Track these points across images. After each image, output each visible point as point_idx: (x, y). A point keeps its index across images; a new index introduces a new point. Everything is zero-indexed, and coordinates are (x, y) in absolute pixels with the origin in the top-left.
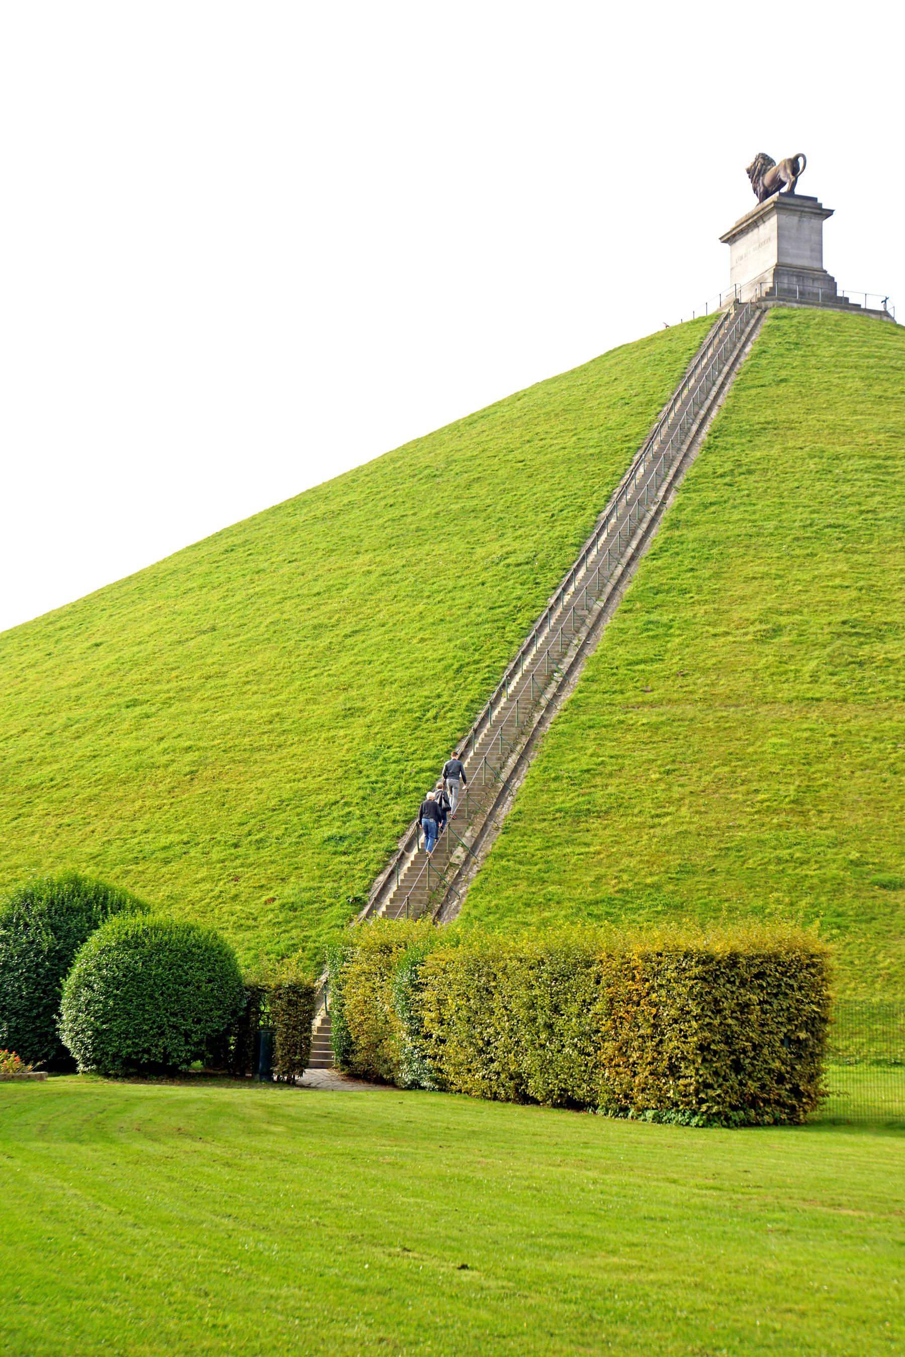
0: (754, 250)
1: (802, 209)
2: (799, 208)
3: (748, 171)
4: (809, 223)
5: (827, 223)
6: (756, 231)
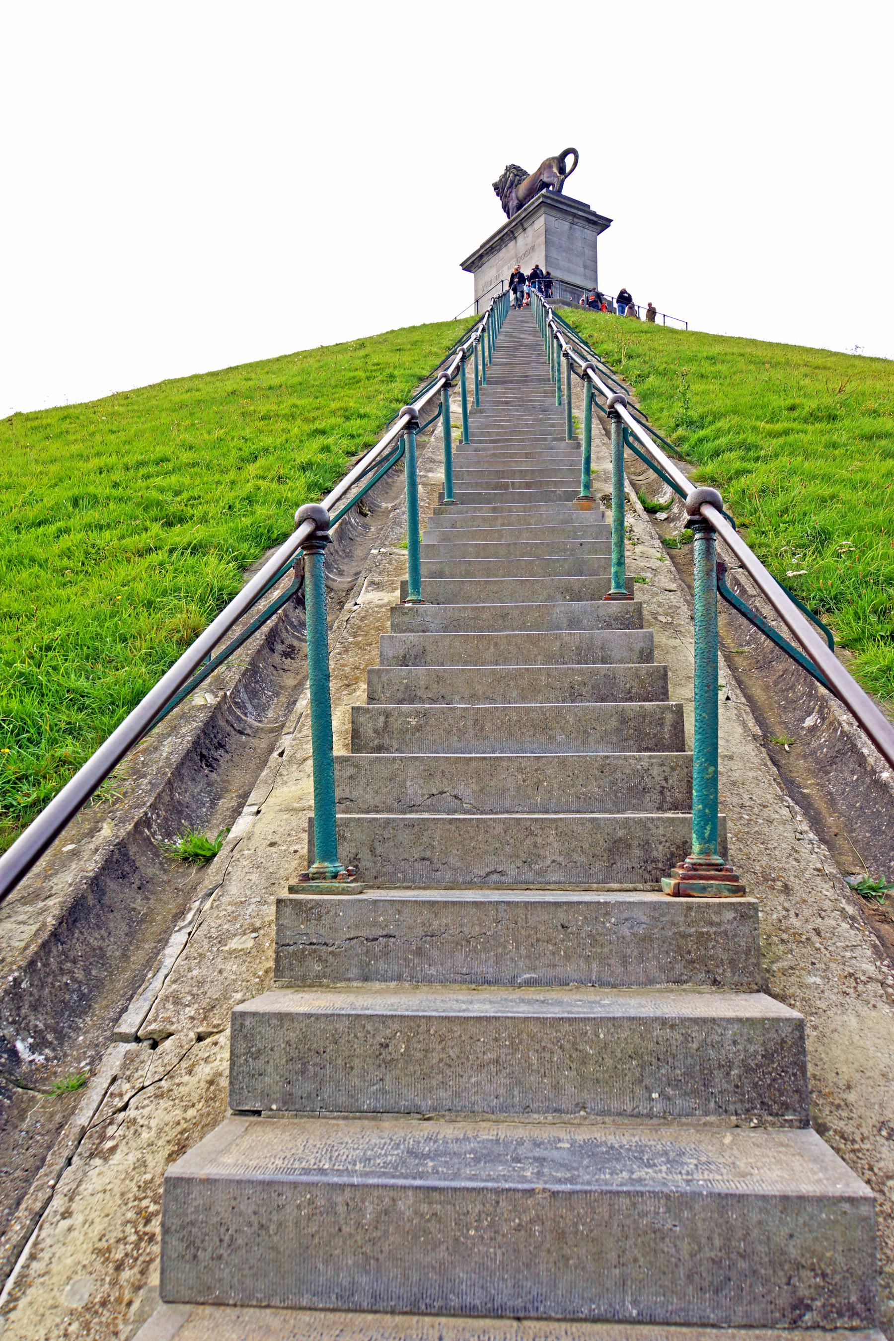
2: (573, 210)
3: (496, 187)
4: (582, 232)
5: (603, 239)
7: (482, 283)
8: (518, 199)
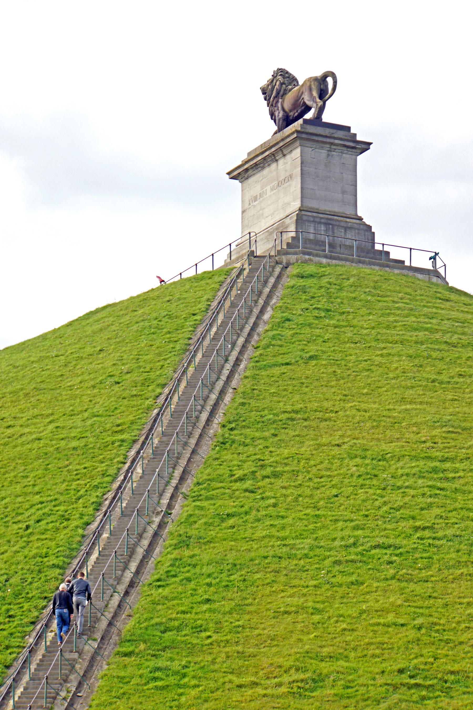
0: (272, 189)
1: (332, 141)
2: (328, 140)
5: (362, 159)
6: (274, 165)
7: (248, 197)
8: (283, 109)
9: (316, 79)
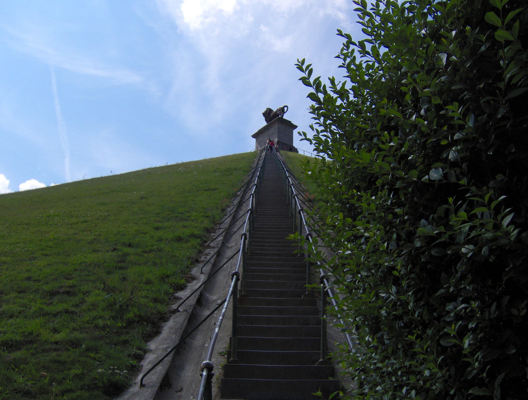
9: (281, 108)
